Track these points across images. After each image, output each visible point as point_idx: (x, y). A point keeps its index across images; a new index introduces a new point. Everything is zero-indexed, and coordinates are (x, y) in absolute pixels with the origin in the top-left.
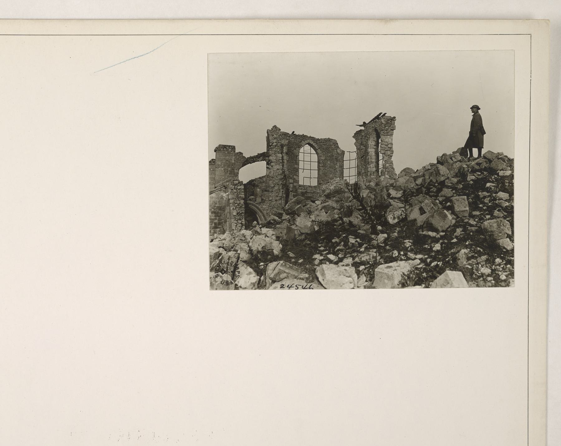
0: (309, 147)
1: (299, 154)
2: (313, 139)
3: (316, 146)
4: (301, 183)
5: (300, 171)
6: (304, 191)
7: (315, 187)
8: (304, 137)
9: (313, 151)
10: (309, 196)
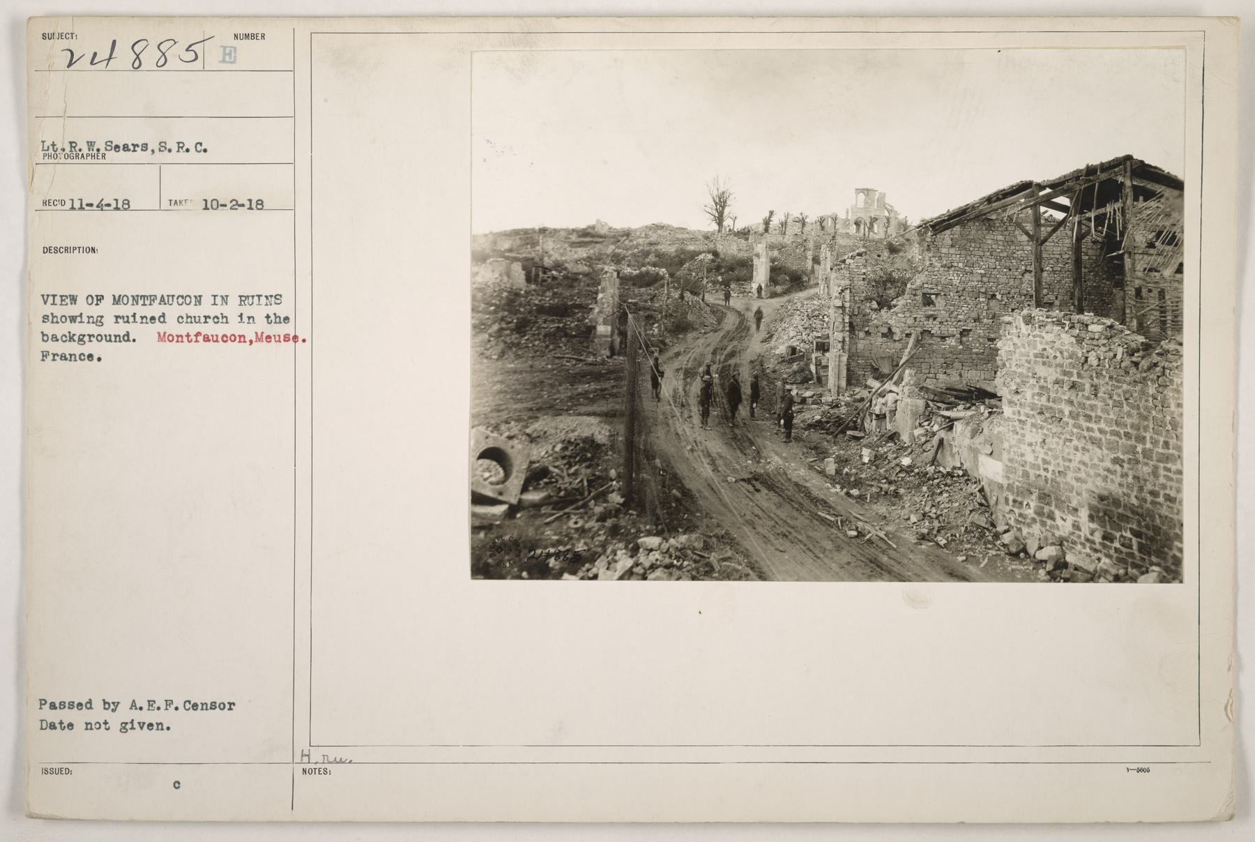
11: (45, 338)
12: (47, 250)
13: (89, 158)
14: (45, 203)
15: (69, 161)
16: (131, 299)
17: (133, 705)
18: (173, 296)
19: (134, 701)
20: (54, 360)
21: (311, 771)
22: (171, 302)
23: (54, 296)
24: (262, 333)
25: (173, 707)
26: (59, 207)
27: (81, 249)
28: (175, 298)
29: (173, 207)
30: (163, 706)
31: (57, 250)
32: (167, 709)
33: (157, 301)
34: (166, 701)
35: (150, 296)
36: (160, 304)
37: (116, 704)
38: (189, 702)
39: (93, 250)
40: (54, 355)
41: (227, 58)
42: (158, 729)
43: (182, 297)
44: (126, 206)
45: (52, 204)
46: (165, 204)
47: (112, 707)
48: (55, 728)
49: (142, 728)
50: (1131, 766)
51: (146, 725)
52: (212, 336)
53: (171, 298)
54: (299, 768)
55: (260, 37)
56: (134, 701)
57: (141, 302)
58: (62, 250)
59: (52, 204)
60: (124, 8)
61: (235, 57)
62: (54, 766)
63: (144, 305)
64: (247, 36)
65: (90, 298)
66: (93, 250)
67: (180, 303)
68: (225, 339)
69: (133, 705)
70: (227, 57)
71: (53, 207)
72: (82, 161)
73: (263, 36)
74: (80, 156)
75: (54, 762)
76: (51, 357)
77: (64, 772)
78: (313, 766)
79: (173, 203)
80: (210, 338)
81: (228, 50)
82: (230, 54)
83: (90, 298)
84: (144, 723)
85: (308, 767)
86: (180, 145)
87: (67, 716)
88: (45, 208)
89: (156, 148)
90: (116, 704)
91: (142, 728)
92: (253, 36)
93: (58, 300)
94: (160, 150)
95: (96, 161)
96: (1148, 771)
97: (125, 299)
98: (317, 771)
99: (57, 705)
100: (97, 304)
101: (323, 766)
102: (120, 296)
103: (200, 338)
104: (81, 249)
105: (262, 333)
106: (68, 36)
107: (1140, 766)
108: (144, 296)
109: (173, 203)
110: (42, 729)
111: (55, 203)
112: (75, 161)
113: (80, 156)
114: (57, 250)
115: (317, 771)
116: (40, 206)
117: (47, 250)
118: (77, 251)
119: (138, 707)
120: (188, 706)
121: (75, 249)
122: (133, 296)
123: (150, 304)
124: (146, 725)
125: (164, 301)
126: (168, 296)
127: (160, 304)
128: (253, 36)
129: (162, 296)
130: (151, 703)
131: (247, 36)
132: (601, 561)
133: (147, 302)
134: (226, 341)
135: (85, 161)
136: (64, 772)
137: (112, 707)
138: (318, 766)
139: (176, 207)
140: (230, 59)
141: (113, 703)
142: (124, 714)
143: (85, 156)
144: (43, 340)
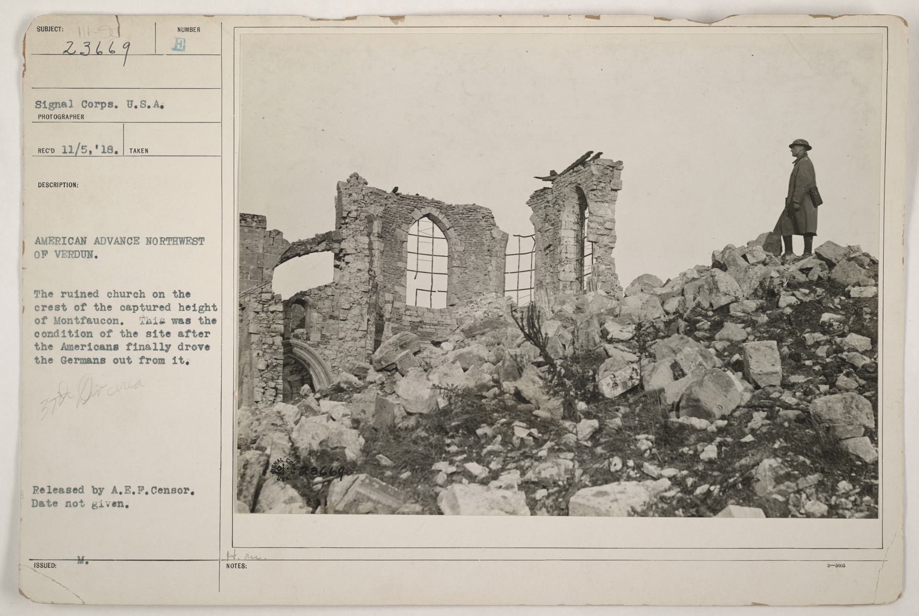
0: (431, 223)
1: (406, 237)
2: (438, 205)
3: (445, 221)
4: (410, 302)
5: (410, 275)
6: (419, 319)
7: (441, 311)
8: (418, 201)
9: (438, 233)
10: (428, 330)
11: (95, 491)
12: (41, 185)
14: (39, 150)
15: (57, 120)
17: (114, 490)
19: (115, 487)
21: (234, 566)
22: (84, 256)
25: (144, 491)
26: (50, 154)
27: (66, 184)
29: (133, 154)
30: (137, 491)
31: (48, 185)
32: (139, 493)
34: (139, 487)
37: (102, 490)
38: (156, 488)
39: (75, 185)
41: (178, 47)
42: (165, 493)
44: (110, 151)
45: (44, 151)
46: (127, 152)
47: (99, 492)
48: (44, 506)
49: (201, 349)
50: (831, 563)
51: (204, 347)
52: (94, 319)
54: (223, 564)
55: (196, 30)
56: (115, 487)
58: (51, 185)
59: (44, 151)
61: (184, 47)
62: (43, 562)
64: (187, 29)
66: (75, 185)
69: (114, 490)
70: (179, 46)
72: (67, 120)
73: (199, 30)
75: (45, 555)
77: (50, 566)
78: (234, 562)
79: (133, 151)
80: (93, 321)
81: (179, 41)
82: (181, 44)
84: (203, 345)
85: (230, 563)
86: (143, 103)
87: (54, 497)
88: (40, 154)
89: (138, 105)
90: (102, 490)
91: (201, 349)
92: (191, 30)
94: (141, 107)
95: (77, 120)
96: (844, 566)
98: (237, 565)
99: (65, 490)
101: (241, 562)
103: (85, 321)
104: (66, 184)
106: (56, 29)
107: (838, 563)
109: (133, 151)
110: (33, 506)
111: (47, 151)
112: (61, 120)
114: (48, 185)
115: (237, 565)
117: (41, 185)
118: (62, 186)
119: (118, 492)
120: (154, 490)
121: (61, 184)
124: (204, 347)
127: (115, 244)
128: (191, 30)
129: (78, 238)
130: (128, 488)
131: (187, 29)
132: (434, 373)
135: (69, 120)
136: (50, 566)
137: (99, 492)
138: (237, 562)
139: (135, 154)
140: (181, 47)
141: (99, 488)
142: (108, 497)
144: (94, 493)
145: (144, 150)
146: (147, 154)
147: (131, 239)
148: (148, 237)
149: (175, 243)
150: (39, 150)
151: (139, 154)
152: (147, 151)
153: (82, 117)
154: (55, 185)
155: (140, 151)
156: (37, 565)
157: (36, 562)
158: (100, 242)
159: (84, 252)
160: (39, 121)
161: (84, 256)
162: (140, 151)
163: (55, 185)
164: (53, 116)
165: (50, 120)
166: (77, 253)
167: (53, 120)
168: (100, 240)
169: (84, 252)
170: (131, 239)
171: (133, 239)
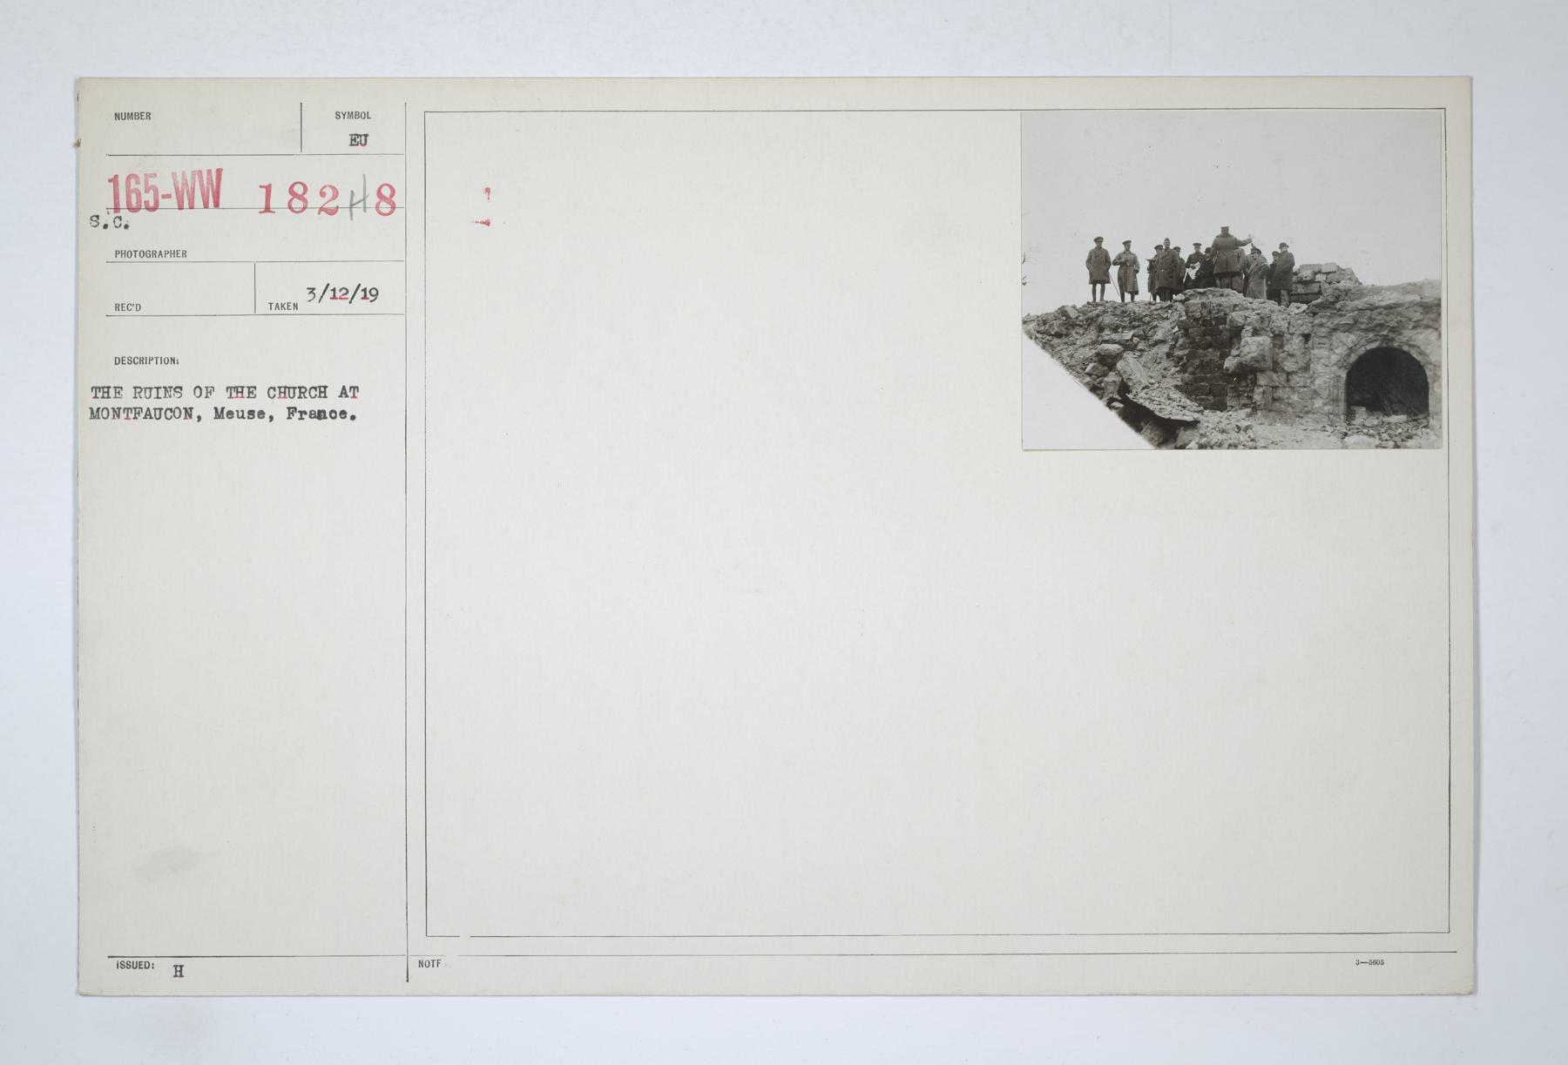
13: (168, 256)
14: (117, 307)
15: (145, 259)
16: (111, 411)
18: (161, 409)
20: (301, 419)
22: (292, 395)
23: (158, 388)
24: (223, 408)
26: (134, 312)
27: (159, 359)
28: (163, 412)
29: (273, 311)
31: (131, 361)
33: (143, 415)
35: (135, 409)
36: (145, 418)
40: (301, 412)
43: (171, 410)
53: (158, 412)
57: (123, 415)
58: (136, 361)
59: (125, 308)
60: (1476, 328)
63: (127, 418)
65: (148, 396)
66: (173, 360)
67: (169, 417)
68: (320, 415)
71: (126, 312)
72: (160, 259)
74: (157, 254)
76: (297, 415)
83: (198, 389)
88: (117, 313)
93: (162, 392)
95: (176, 259)
97: (105, 412)
98: (435, 963)
100: (207, 397)
102: (98, 409)
104: (159, 359)
105: (223, 408)
108: (128, 409)
112: (151, 259)
113: (157, 254)
114: (131, 361)
116: (112, 311)
118: (154, 362)
122: (113, 409)
123: (135, 418)
125: (150, 415)
126: (155, 409)
127: (145, 418)
129: (148, 409)
133: (132, 416)
134: (335, 417)
135: (163, 259)
139: (277, 312)
143: (163, 253)
145: (292, 305)
146: (296, 312)
147: (274, 389)
148: (188, 407)
149: (323, 395)
150: (117, 307)
151: (283, 312)
152: (296, 306)
153: (184, 254)
154: (142, 361)
155: (286, 306)
156: (121, 965)
157: (120, 960)
158: (153, 416)
159: (292, 390)
160: (270, 312)
161: (292, 395)
162: (286, 306)
163: (142, 361)
164: (138, 253)
165: (133, 258)
166: (177, 412)
167: (138, 258)
168: (152, 412)
169: (292, 390)
170: (274, 389)
171: (277, 390)
